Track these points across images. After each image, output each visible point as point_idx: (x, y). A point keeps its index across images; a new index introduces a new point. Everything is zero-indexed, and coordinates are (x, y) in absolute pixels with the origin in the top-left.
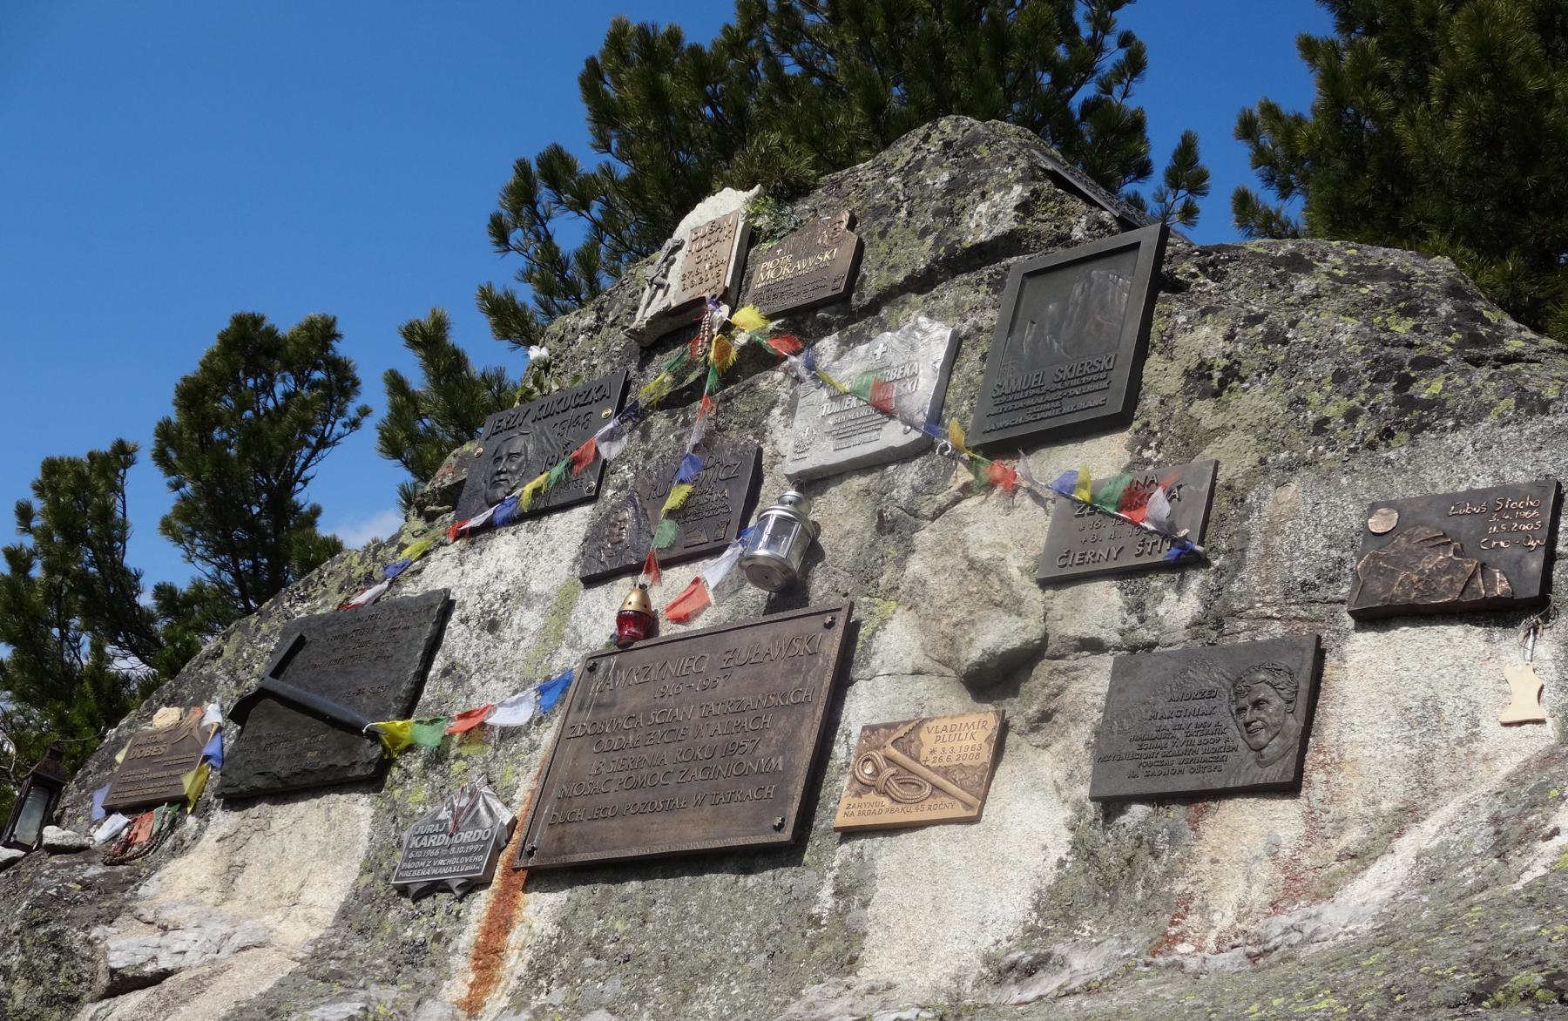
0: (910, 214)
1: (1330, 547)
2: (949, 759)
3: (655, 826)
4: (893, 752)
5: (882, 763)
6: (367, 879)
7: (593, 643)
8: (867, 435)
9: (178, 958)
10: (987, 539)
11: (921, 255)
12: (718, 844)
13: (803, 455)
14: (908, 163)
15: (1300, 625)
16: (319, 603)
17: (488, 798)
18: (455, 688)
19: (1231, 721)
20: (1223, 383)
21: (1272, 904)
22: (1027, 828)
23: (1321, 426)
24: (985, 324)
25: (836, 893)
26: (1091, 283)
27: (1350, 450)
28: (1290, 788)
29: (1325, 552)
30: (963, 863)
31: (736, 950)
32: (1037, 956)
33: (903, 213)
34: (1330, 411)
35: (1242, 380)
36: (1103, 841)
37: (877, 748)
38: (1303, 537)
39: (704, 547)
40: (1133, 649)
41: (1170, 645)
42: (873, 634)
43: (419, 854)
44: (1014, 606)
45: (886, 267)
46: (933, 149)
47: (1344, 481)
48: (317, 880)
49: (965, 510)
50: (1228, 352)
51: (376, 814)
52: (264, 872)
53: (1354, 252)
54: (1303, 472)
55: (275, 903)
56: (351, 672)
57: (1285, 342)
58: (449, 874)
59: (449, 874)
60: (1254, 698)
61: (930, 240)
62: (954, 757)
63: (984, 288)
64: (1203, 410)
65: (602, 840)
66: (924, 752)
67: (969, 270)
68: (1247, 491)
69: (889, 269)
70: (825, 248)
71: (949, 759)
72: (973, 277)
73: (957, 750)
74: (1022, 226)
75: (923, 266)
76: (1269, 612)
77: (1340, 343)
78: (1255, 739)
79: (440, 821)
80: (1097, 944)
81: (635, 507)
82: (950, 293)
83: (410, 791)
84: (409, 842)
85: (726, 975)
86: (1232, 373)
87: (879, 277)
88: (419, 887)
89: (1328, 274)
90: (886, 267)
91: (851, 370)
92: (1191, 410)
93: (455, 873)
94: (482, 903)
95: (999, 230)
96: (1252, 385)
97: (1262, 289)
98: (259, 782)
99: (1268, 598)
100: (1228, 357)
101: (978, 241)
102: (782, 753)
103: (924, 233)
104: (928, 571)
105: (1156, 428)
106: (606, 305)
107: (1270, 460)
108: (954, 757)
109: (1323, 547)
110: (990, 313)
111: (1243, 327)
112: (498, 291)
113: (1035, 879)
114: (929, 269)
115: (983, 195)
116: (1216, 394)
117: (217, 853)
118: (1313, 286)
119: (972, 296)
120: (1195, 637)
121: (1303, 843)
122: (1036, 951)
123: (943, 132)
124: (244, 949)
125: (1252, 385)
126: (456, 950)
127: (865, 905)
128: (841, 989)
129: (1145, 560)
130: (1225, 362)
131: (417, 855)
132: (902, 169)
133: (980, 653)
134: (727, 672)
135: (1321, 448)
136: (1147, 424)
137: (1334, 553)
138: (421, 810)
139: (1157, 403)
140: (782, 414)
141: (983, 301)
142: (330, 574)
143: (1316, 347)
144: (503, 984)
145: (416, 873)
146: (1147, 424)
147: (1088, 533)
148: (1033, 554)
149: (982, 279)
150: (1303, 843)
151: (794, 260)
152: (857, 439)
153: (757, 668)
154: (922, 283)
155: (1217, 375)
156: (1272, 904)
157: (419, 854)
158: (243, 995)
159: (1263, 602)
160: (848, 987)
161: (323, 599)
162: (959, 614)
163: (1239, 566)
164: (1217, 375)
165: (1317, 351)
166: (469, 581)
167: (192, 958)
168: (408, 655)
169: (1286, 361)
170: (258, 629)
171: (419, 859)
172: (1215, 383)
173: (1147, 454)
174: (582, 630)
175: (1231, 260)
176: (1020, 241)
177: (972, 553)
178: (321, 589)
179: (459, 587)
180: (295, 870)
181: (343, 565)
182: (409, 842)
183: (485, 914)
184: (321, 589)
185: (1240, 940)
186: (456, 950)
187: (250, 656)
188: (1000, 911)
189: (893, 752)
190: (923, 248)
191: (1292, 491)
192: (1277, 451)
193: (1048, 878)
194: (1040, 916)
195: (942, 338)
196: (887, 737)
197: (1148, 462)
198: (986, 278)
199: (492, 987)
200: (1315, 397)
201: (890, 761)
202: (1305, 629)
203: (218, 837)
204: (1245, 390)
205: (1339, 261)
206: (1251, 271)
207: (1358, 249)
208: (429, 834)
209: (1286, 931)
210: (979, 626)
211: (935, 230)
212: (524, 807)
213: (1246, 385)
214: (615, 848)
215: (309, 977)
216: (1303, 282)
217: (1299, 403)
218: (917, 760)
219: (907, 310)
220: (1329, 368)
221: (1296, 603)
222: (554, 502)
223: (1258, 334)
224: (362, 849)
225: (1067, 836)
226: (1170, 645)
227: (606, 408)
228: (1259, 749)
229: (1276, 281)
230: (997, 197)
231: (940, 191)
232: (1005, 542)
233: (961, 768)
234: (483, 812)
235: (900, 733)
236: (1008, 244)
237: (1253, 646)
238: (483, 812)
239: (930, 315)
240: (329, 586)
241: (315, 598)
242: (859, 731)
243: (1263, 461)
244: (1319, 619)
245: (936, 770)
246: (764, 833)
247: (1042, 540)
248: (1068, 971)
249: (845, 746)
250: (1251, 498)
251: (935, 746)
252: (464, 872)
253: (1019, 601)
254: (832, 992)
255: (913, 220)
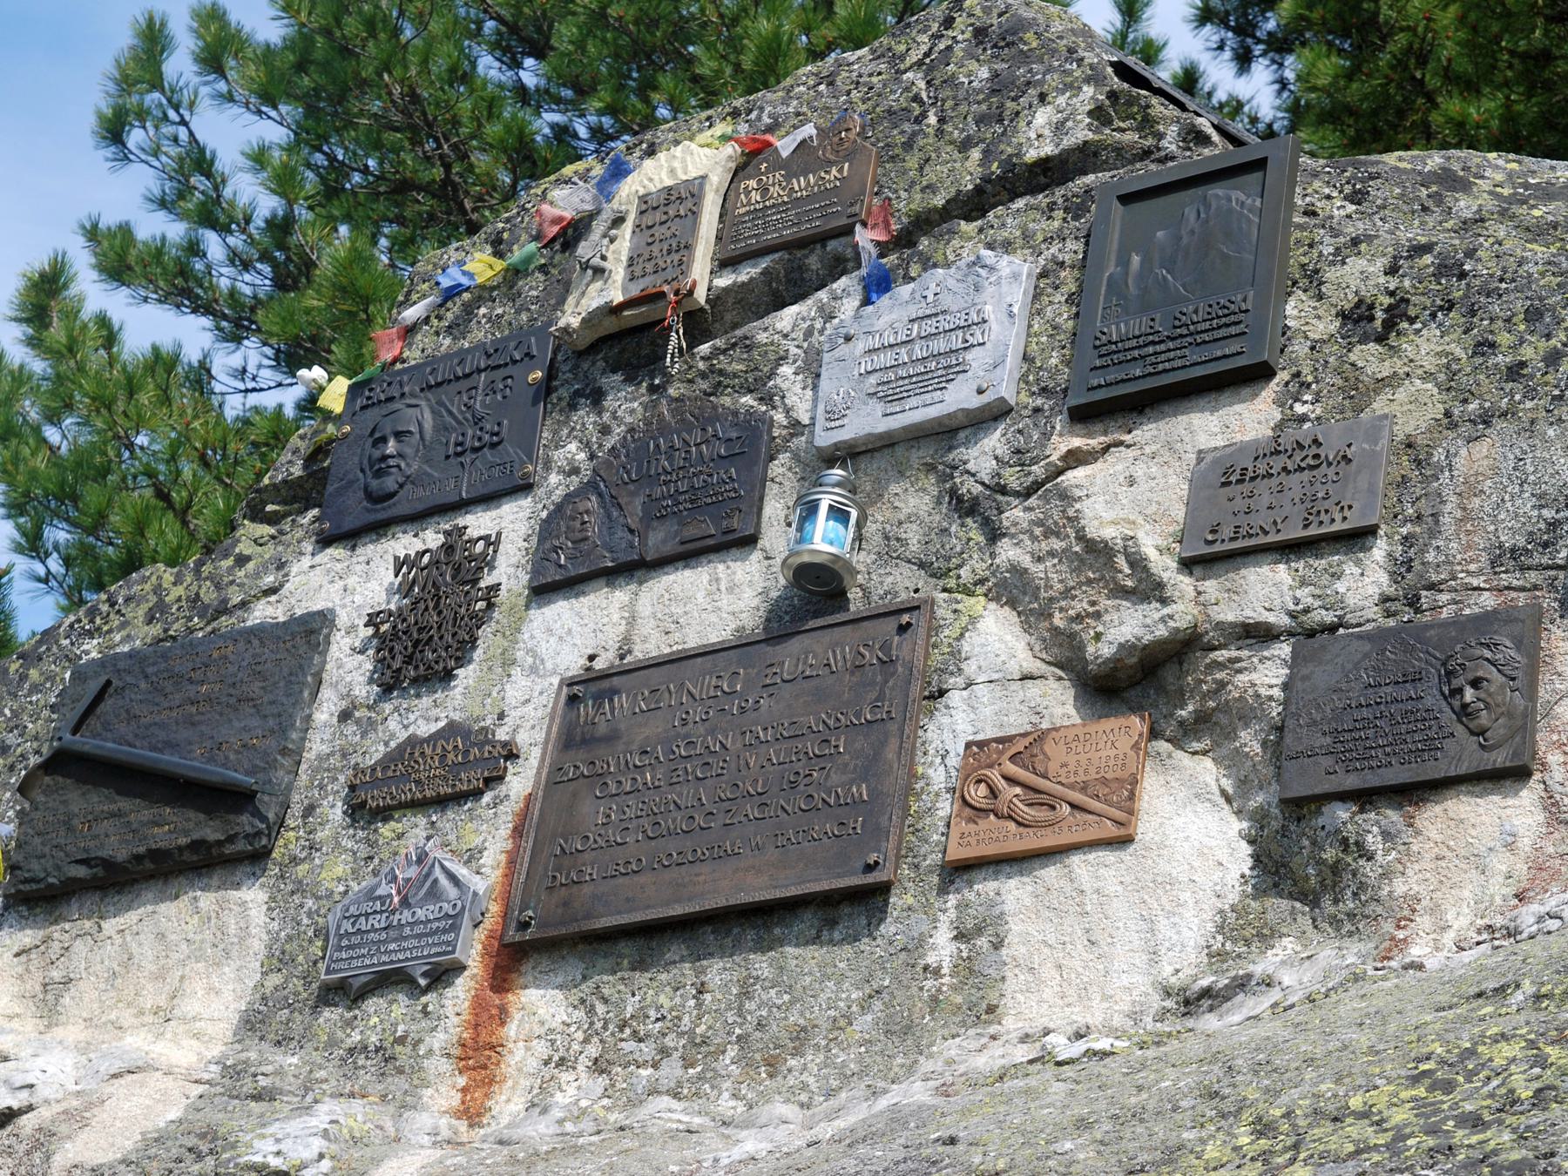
0: (942, 120)
1: (1541, 507)
2: (1086, 771)
3: (701, 878)
4: (1012, 769)
5: (1001, 783)
6: (275, 979)
7: (563, 667)
8: (928, 396)
9: (24, 1094)
10: (1108, 515)
11: (969, 171)
12: (793, 891)
13: (837, 423)
14: (927, 55)
15: (1514, 594)
16: (118, 638)
17: (447, 864)
18: (364, 735)
19: (1444, 704)
20: (1389, 325)
21: (1516, 896)
22: (1196, 844)
23: (1515, 371)
24: (1067, 258)
25: (956, 938)
26: (1208, 206)
27: (1554, 398)
28: (1515, 774)
29: (1535, 513)
30: (1119, 888)
31: (832, 1013)
32: (1234, 978)
33: (932, 119)
34: (1527, 353)
35: (1412, 321)
36: (1296, 849)
37: (991, 766)
38: (1507, 497)
39: (711, 542)
40: (1311, 634)
41: (1359, 625)
42: (962, 635)
43: (356, 940)
44: (1150, 590)
45: (918, 188)
46: (960, 38)
47: (1551, 432)
48: (199, 986)
49: (1073, 482)
50: (1392, 288)
51: (273, 899)
52: (102, 986)
53: (1514, 166)
54: (1500, 424)
55: (136, 1022)
56: (200, 723)
57: (1462, 275)
58: (413, 959)
59: (407, 959)
60: (1471, 676)
61: (976, 154)
62: (1092, 771)
63: (1059, 214)
64: (1369, 359)
65: (628, 900)
66: (1053, 768)
67: (1033, 190)
68: (1434, 448)
69: (923, 190)
70: (831, 163)
71: (1086, 771)
72: (1041, 199)
73: (1096, 762)
74: (1096, 137)
75: (970, 187)
76: (1475, 583)
77: (1530, 275)
78: (1476, 722)
79: (380, 897)
80: (1309, 957)
81: (600, 495)
82: (1012, 217)
83: (322, 866)
84: (339, 927)
85: (823, 1043)
86: (1398, 312)
87: (910, 200)
88: (364, 979)
89: (1491, 193)
90: (918, 188)
91: (894, 316)
92: (1353, 357)
93: (417, 958)
94: (459, 995)
95: (1068, 142)
96: (1425, 325)
97: (1413, 212)
98: (81, 872)
99: (1473, 567)
100: (1392, 294)
101: (1042, 154)
102: (865, 780)
103: (965, 146)
104: (1028, 558)
105: (1310, 379)
106: (505, 235)
107: (1456, 412)
108: (1092, 771)
109: (1534, 507)
110: (1071, 245)
111: (1406, 258)
112: (109, 220)
113: (1214, 899)
114: (978, 190)
115: (1042, 98)
116: (1381, 339)
117: (20, 969)
118: (1475, 208)
119: (1044, 224)
120: (1389, 614)
121: (1544, 830)
122: (1233, 973)
123: (970, 15)
124: (114, 1076)
125: (1425, 325)
126: (430, 1052)
127: (997, 946)
128: (984, 1040)
129: (1313, 531)
130: (1387, 301)
131: (352, 940)
132: (920, 63)
133: (1113, 649)
134: (771, 690)
135: (1517, 397)
136: (1298, 374)
137: (1546, 513)
138: (341, 889)
139: (1307, 350)
140: (796, 373)
141: (1061, 229)
142: (128, 600)
143: (1501, 280)
144: (510, 1083)
145: (355, 963)
146: (1298, 374)
147: (1240, 504)
148: (1171, 529)
149: (1055, 203)
150: (1544, 830)
151: (788, 178)
152: (913, 402)
153: (814, 682)
154: (974, 205)
155: (1380, 315)
156: (1516, 896)
157: (356, 940)
158: (150, 1126)
159: (1467, 572)
160: (994, 1038)
161: (124, 633)
162: (1080, 606)
163: (1434, 533)
164: (1380, 315)
165: (1504, 285)
166: (358, 599)
167: (43, 1092)
168: (288, 695)
169: (1466, 296)
170: (23, 678)
171: (359, 946)
172: (1378, 323)
173: (1299, 409)
174: (543, 650)
175: (1371, 178)
176: (1096, 154)
177: (1092, 532)
178: (116, 621)
179: (344, 606)
180: (160, 976)
181: (148, 587)
182: (339, 927)
183: (467, 1004)
184: (116, 621)
185: (1485, 936)
186: (430, 1052)
187: (15, 714)
188: (1175, 937)
189: (1012, 769)
190: (968, 164)
191: (1481, 448)
192: (1465, 401)
193: (1231, 896)
194: (1226, 938)
195: (1015, 276)
196: (1001, 753)
197: (1303, 419)
198: (1060, 201)
199: (496, 1088)
200: (1504, 339)
201: (1011, 780)
202: (1522, 599)
203: (16, 949)
204: (1418, 331)
205: (1499, 177)
206: (1398, 191)
207: (1519, 162)
208: (367, 915)
209: (1540, 920)
210: (1107, 618)
211: (983, 141)
212: (499, 872)
213: (1418, 326)
214: (648, 907)
215: (231, 1097)
216: (1462, 203)
217: (1485, 346)
218: (1045, 777)
219: (956, 243)
220: (1520, 306)
221: (1506, 572)
222: (401, 507)
223: (1427, 266)
224: (258, 945)
225: (1245, 849)
226: (1359, 625)
227: (533, 370)
228: (1482, 732)
229: (1430, 203)
230: (1062, 100)
231: (981, 91)
232: (1132, 517)
233: (1104, 781)
234: (444, 881)
235: (1020, 746)
236: (1083, 158)
237: (1458, 623)
238: (444, 881)
239: (990, 246)
240: (129, 616)
241: (110, 631)
242: (961, 750)
243: (1448, 414)
244: (1536, 587)
245: (1071, 787)
246: (853, 874)
247: (1179, 513)
248: (1278, 988)
249: (942, 768)
250: (1439, 455)
251: (1064, 759)
252: (430, 956)
253: (1160, 585)
254: (974, 1045)
255: (948, 128)
